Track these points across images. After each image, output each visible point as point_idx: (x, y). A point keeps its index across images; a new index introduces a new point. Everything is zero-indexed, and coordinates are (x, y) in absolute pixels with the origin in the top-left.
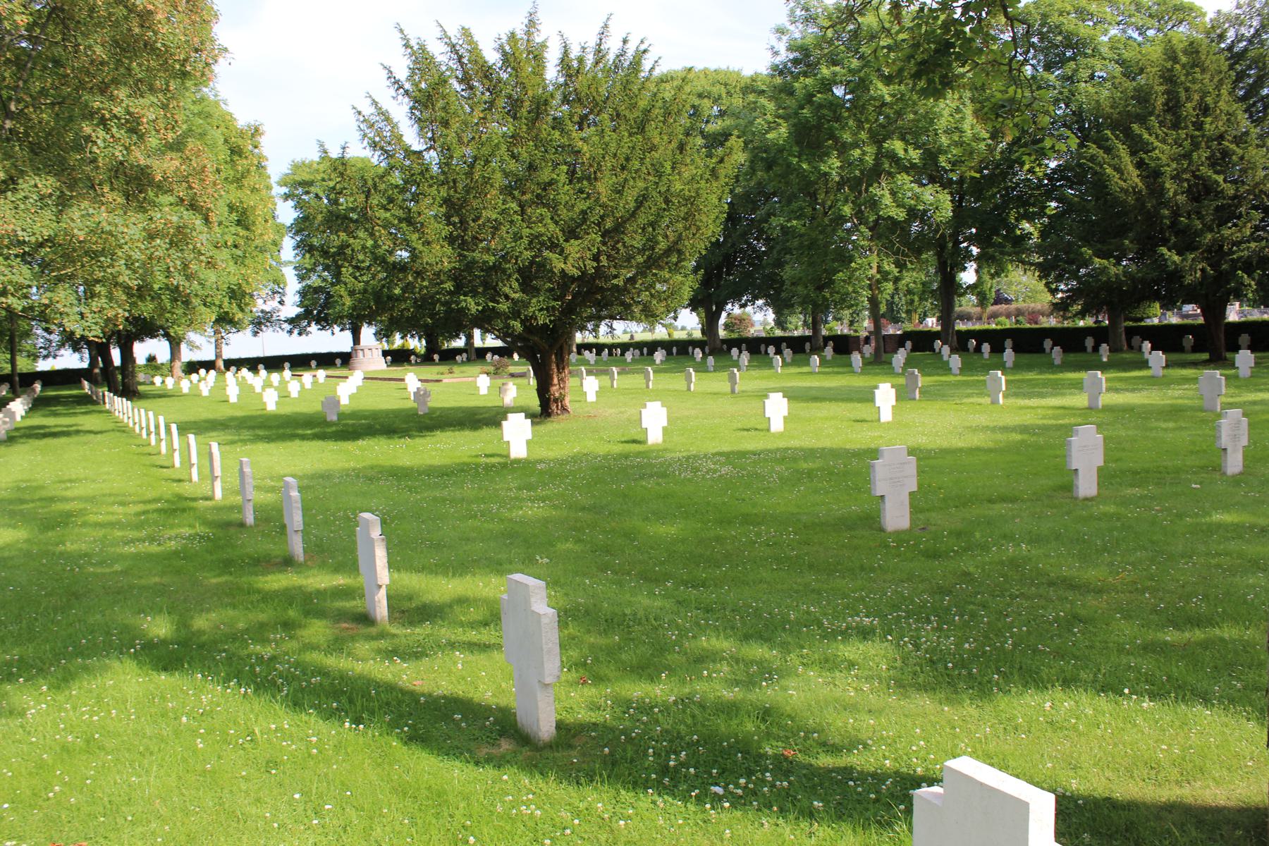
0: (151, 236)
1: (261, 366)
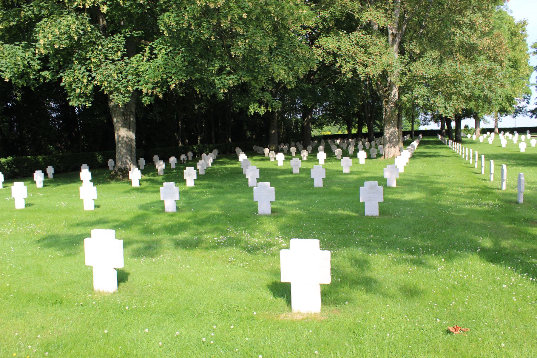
0: (476, 74)
1: (515, 132)
